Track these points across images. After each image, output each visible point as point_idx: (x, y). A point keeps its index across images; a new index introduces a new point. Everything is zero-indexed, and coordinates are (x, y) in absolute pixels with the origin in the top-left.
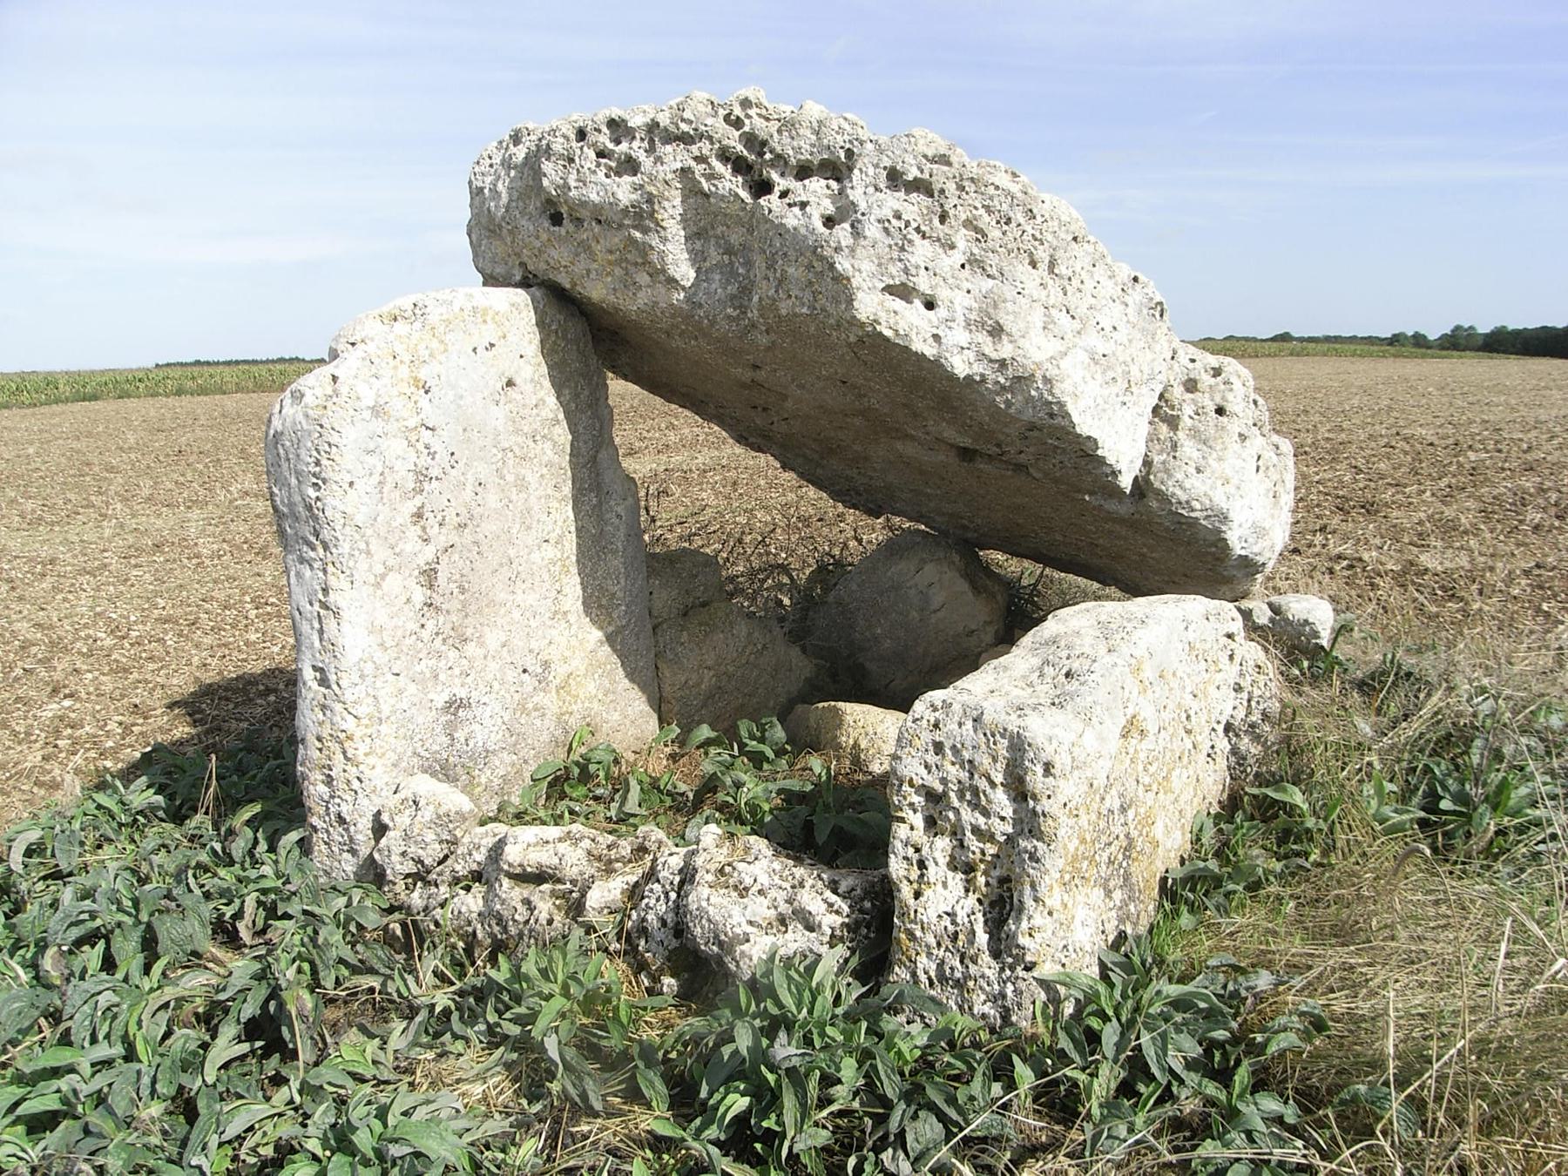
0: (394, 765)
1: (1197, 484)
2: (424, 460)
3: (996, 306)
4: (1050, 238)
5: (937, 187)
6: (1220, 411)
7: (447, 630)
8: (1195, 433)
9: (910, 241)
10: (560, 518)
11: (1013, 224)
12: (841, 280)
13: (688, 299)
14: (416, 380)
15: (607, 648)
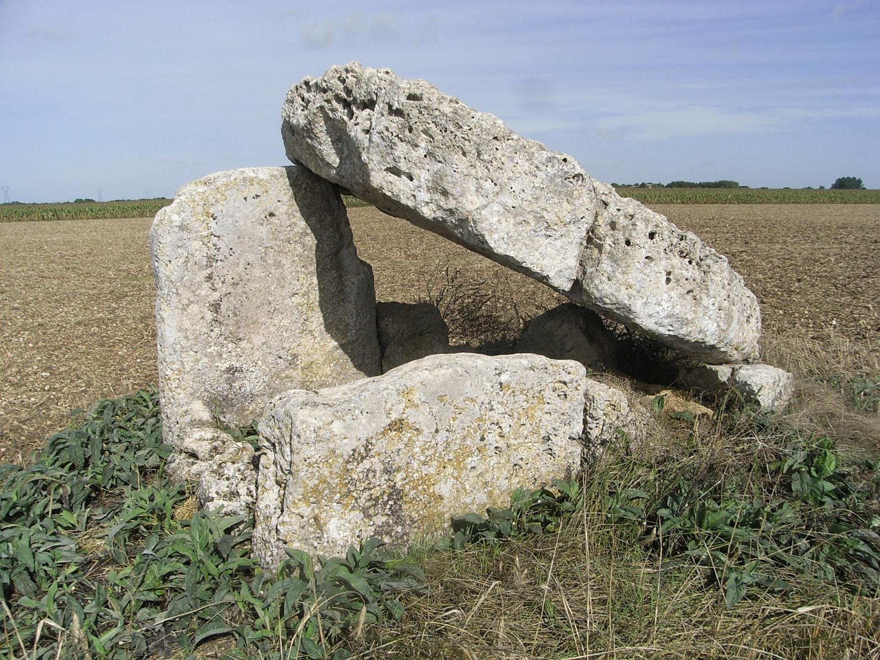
0: (191, 394)
1: (606, 287)
2: (213, 251)
3: (441, 179)
4: (475, 138)
5: (406, 112)
6: (628, 243)
7: (227, 333)
8: (612, 257)
9: (394, 144)
10: (308, 283)
11: (448, 132)
12: (364, 165)
13: (337, 173)
14: (207, 213)
15: (340, 351)
